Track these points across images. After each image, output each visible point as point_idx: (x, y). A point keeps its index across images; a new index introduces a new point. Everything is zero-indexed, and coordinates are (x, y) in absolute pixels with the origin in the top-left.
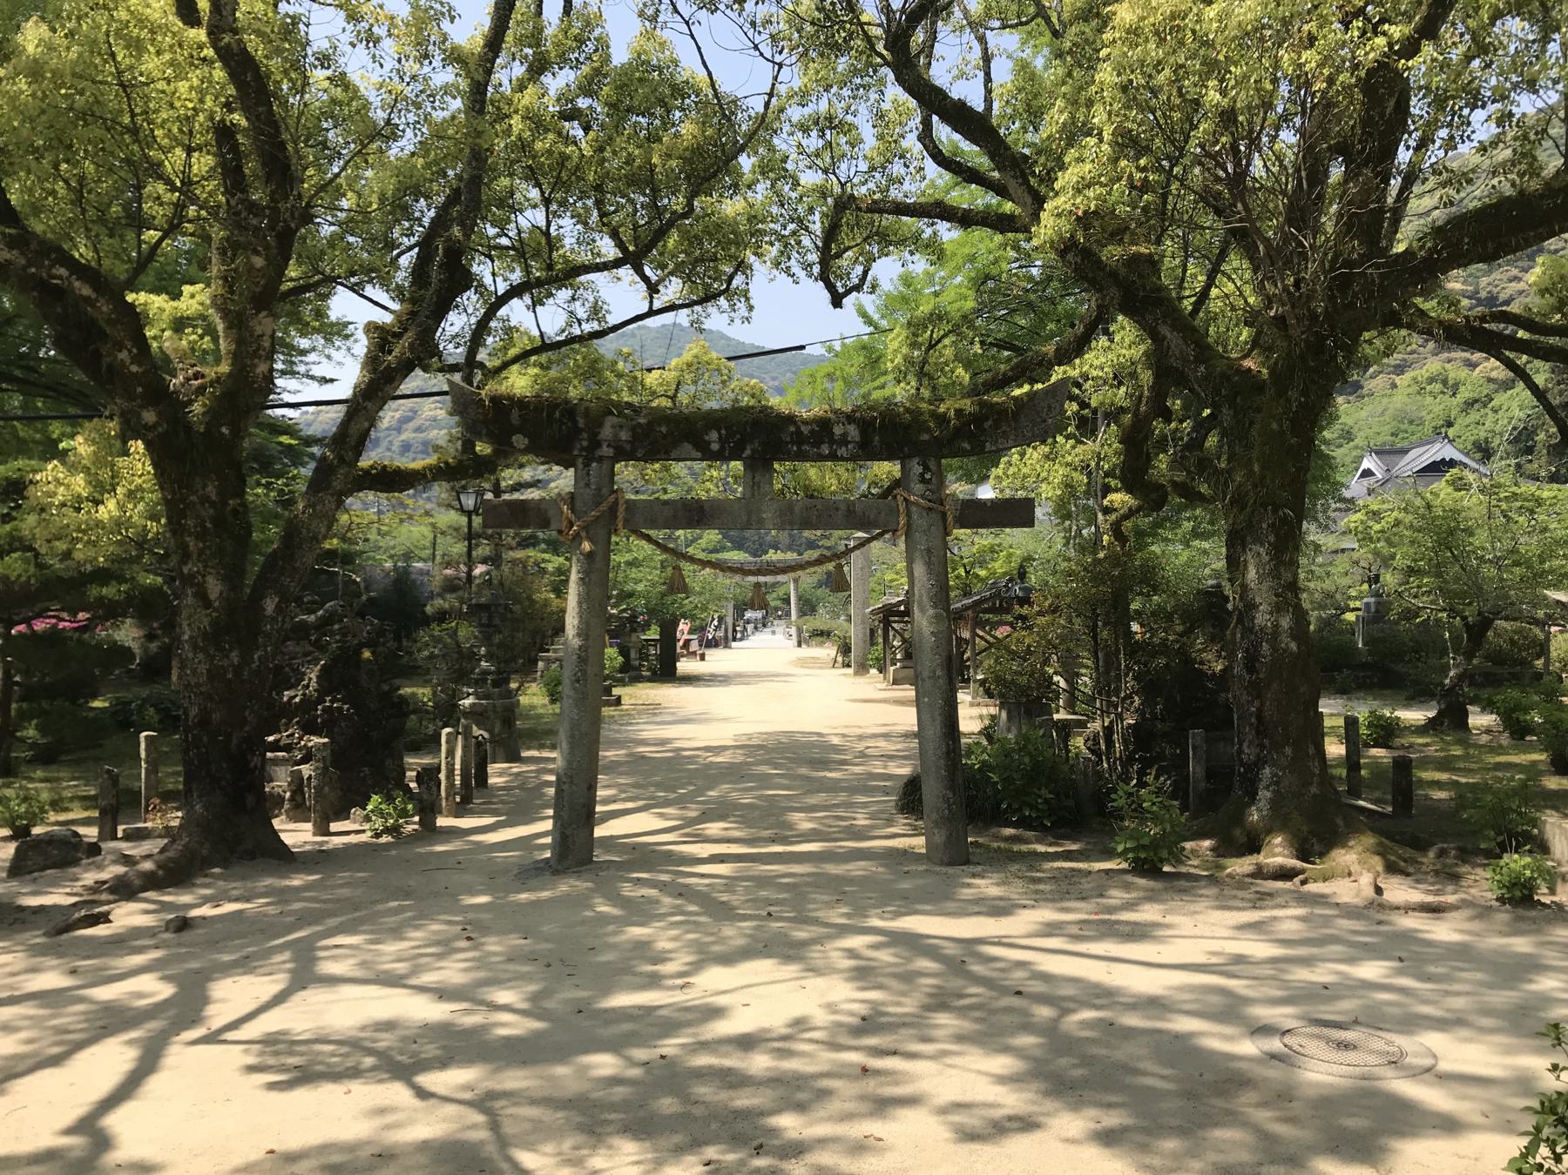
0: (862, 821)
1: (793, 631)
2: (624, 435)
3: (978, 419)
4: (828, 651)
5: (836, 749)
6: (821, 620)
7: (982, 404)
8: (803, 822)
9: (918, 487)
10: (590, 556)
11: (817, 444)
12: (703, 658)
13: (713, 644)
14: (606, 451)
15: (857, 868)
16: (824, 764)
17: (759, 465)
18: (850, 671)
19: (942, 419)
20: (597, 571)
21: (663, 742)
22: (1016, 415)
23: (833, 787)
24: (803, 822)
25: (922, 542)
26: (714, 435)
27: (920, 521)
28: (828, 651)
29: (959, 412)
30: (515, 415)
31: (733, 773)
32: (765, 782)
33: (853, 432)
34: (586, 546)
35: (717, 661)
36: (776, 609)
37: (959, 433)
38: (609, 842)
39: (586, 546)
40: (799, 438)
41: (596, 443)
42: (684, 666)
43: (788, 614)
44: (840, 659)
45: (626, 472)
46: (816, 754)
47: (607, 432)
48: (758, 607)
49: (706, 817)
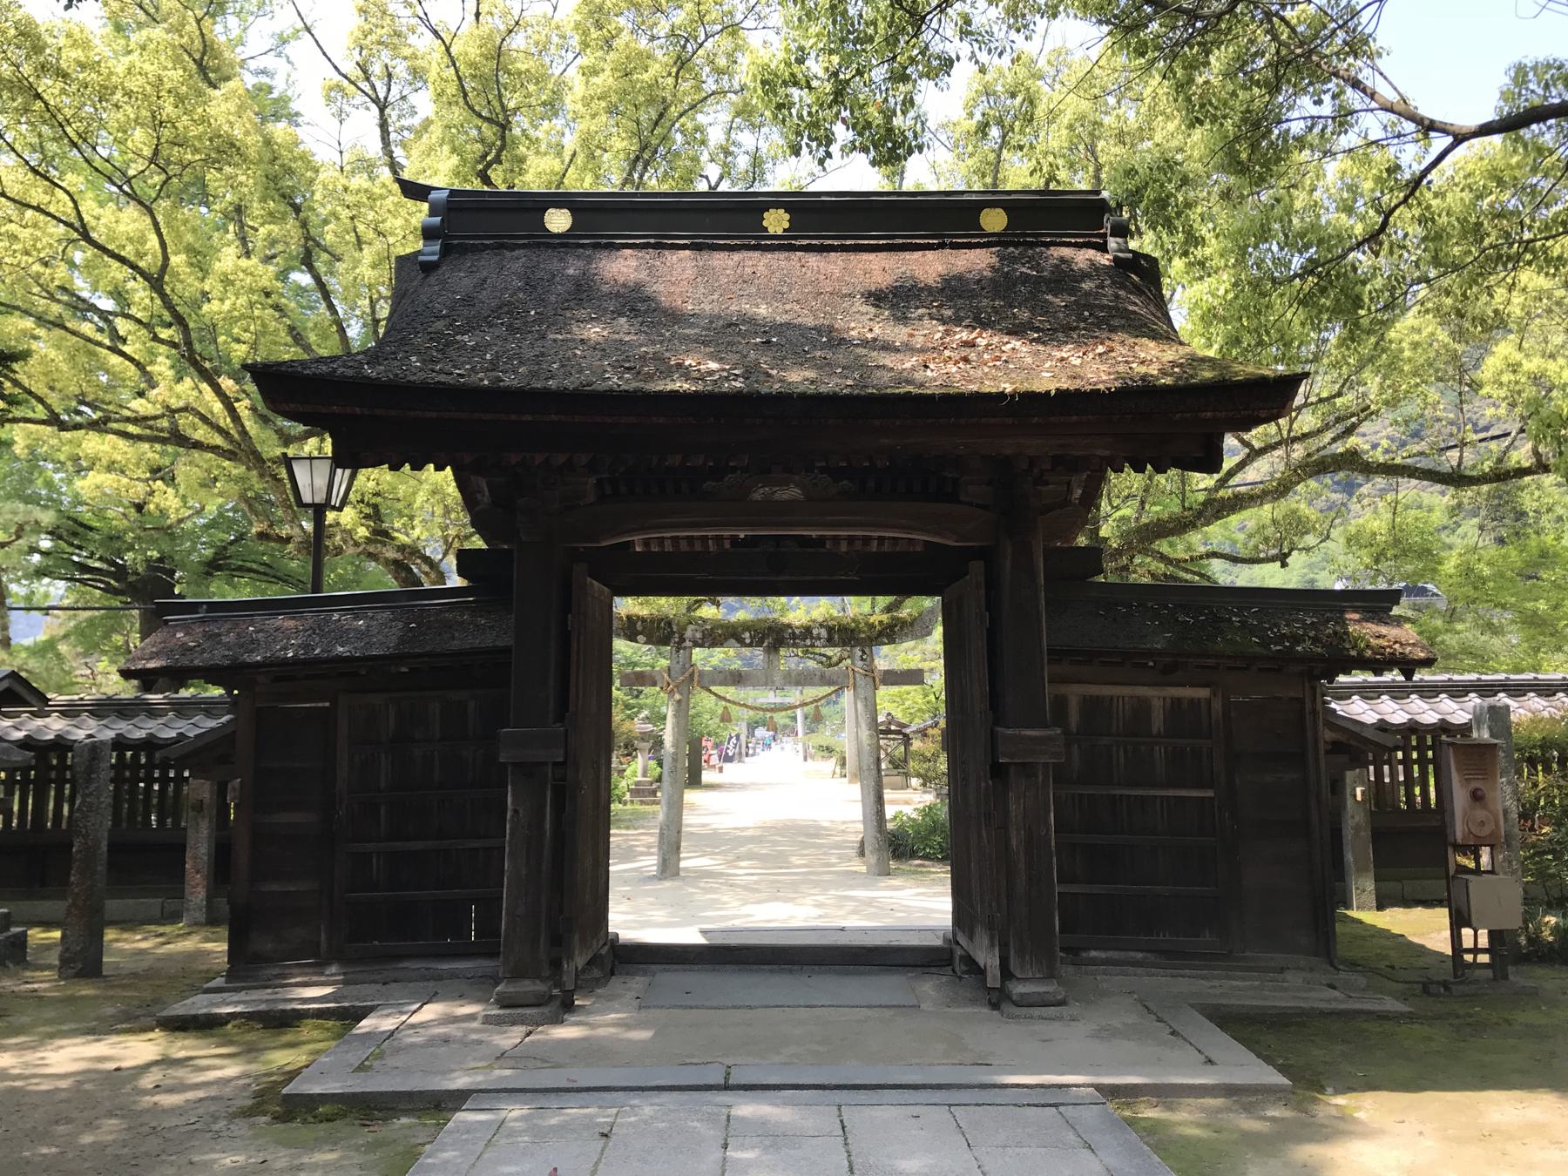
0: (834, 861)
1: (800, 747)
2: (698, 635)
3: (891, 626)
4: (831, 764)
5: (826, 829)
6: (825, 736)
7: (893, 618)
8: (795, 860)
9: (860, 663)
10: (679, 702)
11: (804, 639)
12: (721, 770)
13: (729, 759)
14: (688, 644)
15: (826, 877)
16: (817, 836)
17: (774, 648)
18: (845, 780)
19: (872, 626)
20: (682, 708)
21: (704, 825)
22: (912, 624)
23: (821, 846)
24: (795, 860)
25: (862, 692)
26: (747, 635)
27: (861, 681)
28: (831, 764)
29: (881, 622)
30: (639, 626)
31: (752, 839)
32: (776, 843)
33: (824, 633)
34: (677, 697)
35: (732, 772)
36: (786, 726)
37: (880, 634)
38: (686, 869)
39: (677, 697)
40: (794, 636)
41: (682, 640)
42: (707, 776)
43: (794, 732)
44: (838, 770)
45: (698, 653)
46: (812, 831)
47: (688, 634)
48: (770, 723)
49: (739, 858)
